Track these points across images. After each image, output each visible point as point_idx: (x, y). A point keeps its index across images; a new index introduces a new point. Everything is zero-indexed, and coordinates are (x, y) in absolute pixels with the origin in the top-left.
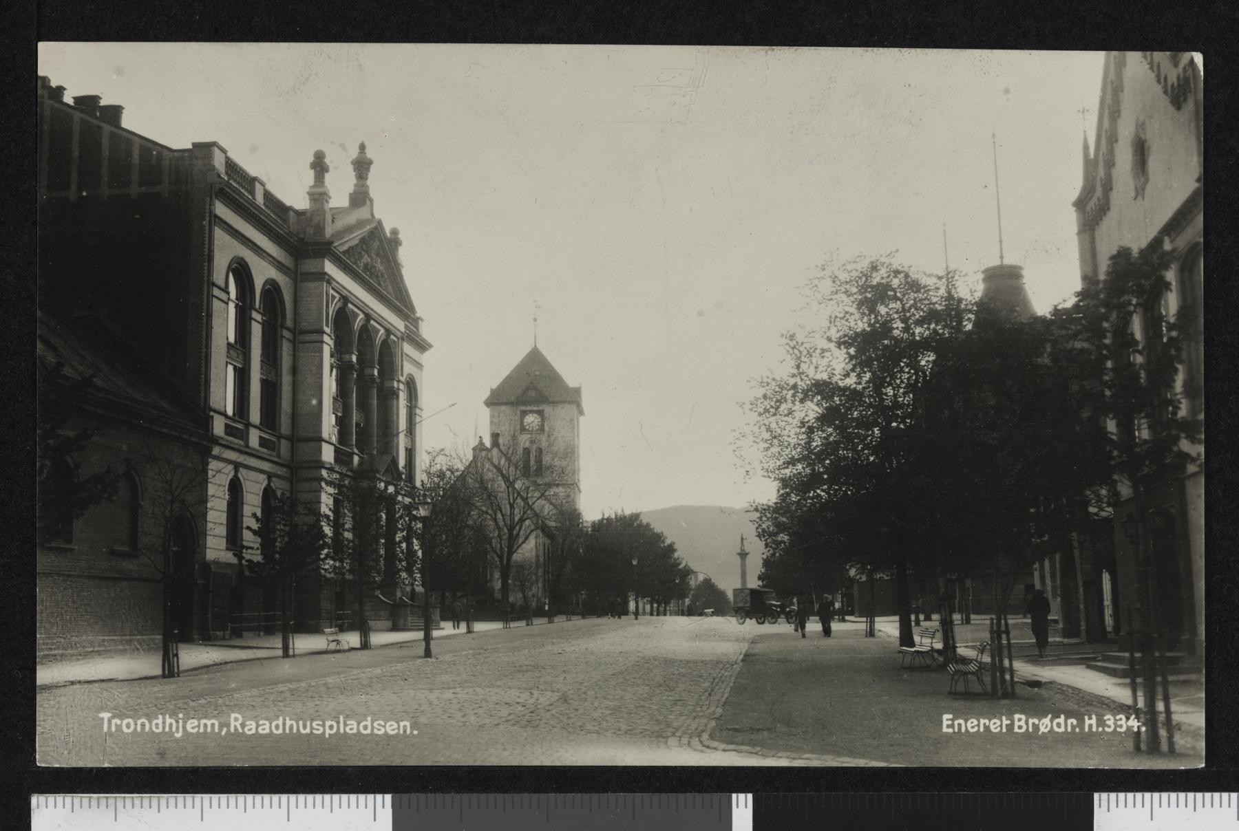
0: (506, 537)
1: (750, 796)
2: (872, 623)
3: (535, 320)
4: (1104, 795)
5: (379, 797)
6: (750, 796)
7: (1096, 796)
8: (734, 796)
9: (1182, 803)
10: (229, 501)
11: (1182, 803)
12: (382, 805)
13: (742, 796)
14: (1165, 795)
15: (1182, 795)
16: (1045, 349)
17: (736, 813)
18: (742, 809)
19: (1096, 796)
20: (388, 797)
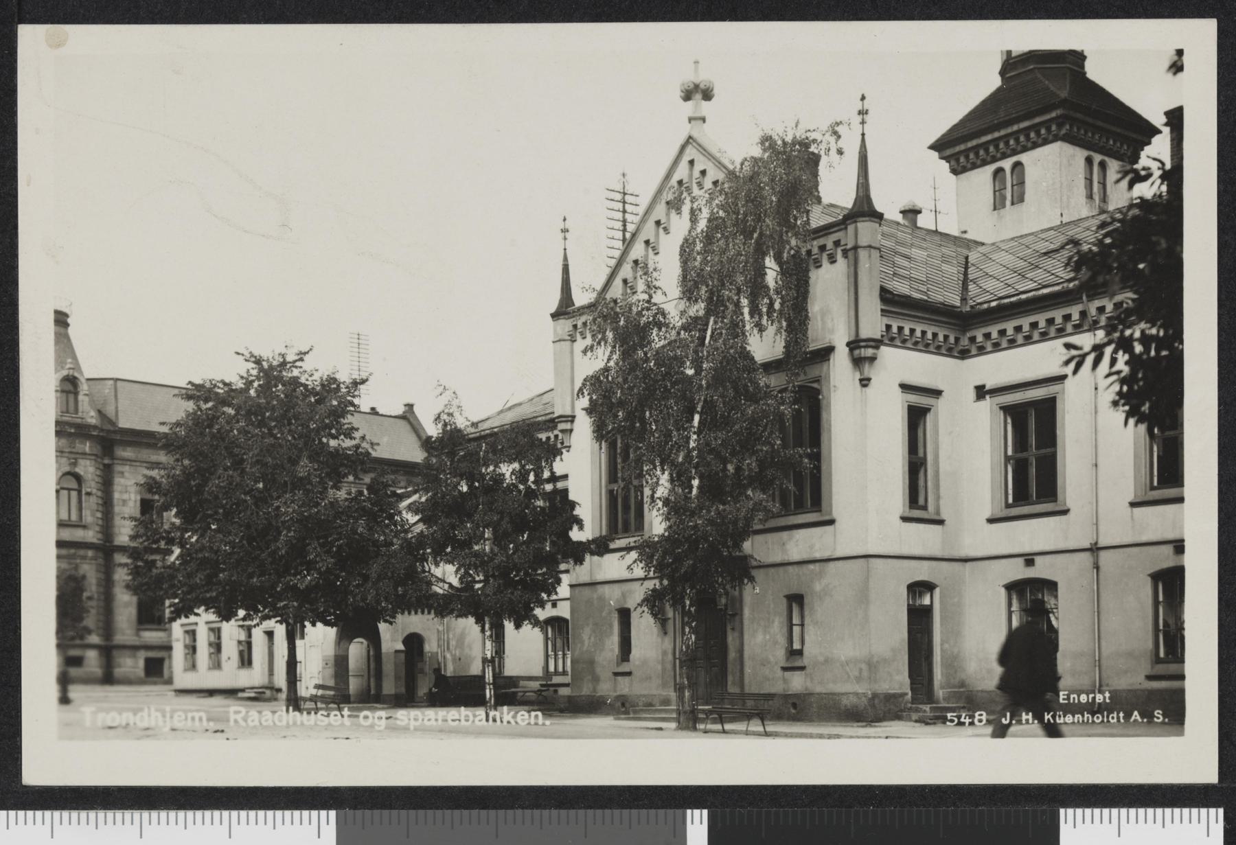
0: (90, 621)
1: (705, 812)
2: (499, 638)
3: (696, 62)
4: (1070, 811)
5: (323, 813)
6: (705, 812)
7: (1062, 811)
8: (689, 812)
9: (30, 820)
10: (72, 584)
11: (30, 820)
12: (328, 820)
13: (697, 812)
14: (243, 813)
15: (261, 813)
16: (257, 391)
17: (690, 829)
18: (697, 826)
19: (1062, 811)
20: (333, 813)
